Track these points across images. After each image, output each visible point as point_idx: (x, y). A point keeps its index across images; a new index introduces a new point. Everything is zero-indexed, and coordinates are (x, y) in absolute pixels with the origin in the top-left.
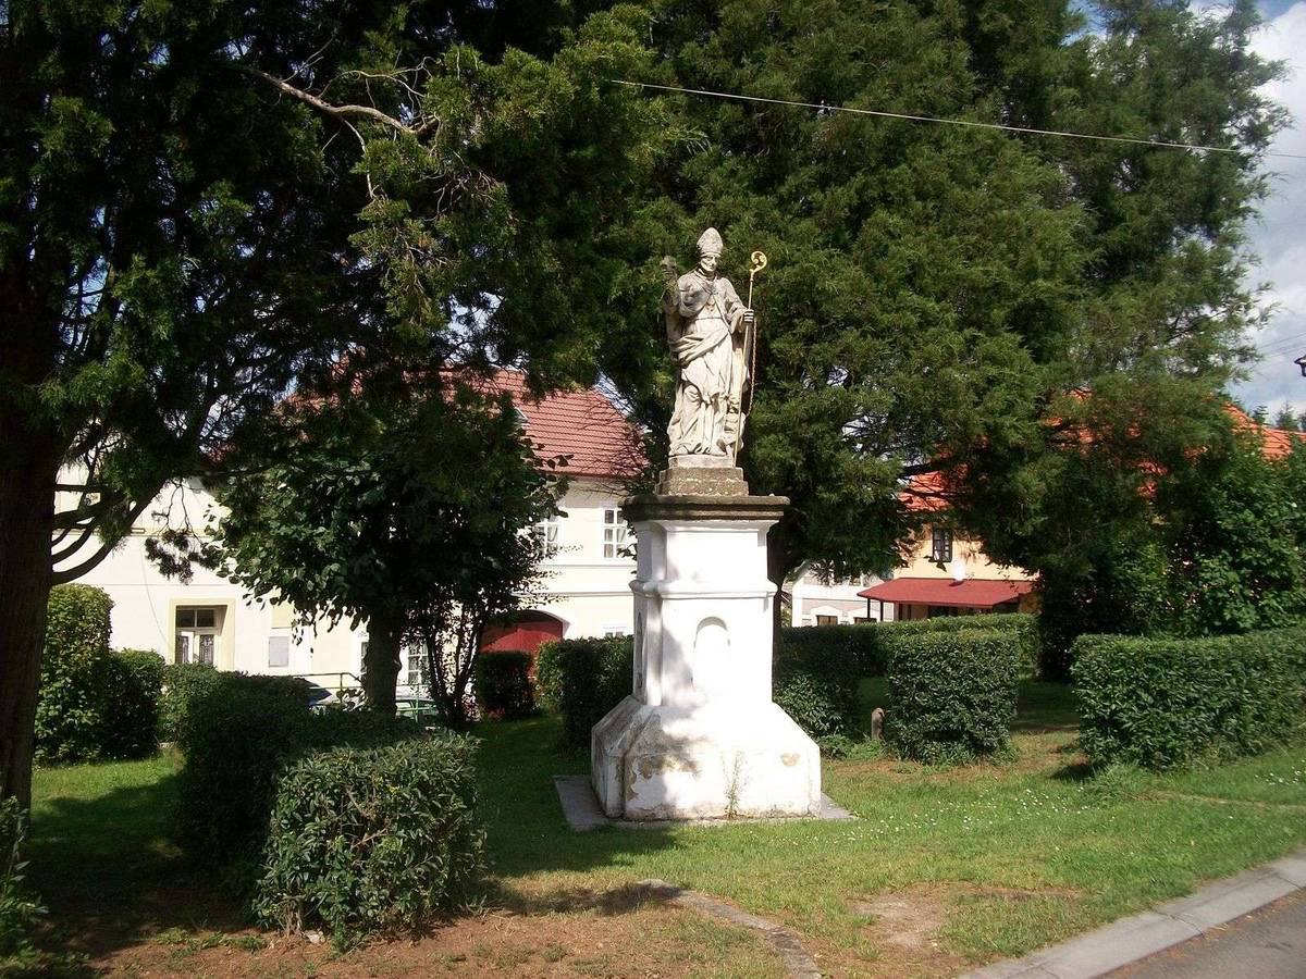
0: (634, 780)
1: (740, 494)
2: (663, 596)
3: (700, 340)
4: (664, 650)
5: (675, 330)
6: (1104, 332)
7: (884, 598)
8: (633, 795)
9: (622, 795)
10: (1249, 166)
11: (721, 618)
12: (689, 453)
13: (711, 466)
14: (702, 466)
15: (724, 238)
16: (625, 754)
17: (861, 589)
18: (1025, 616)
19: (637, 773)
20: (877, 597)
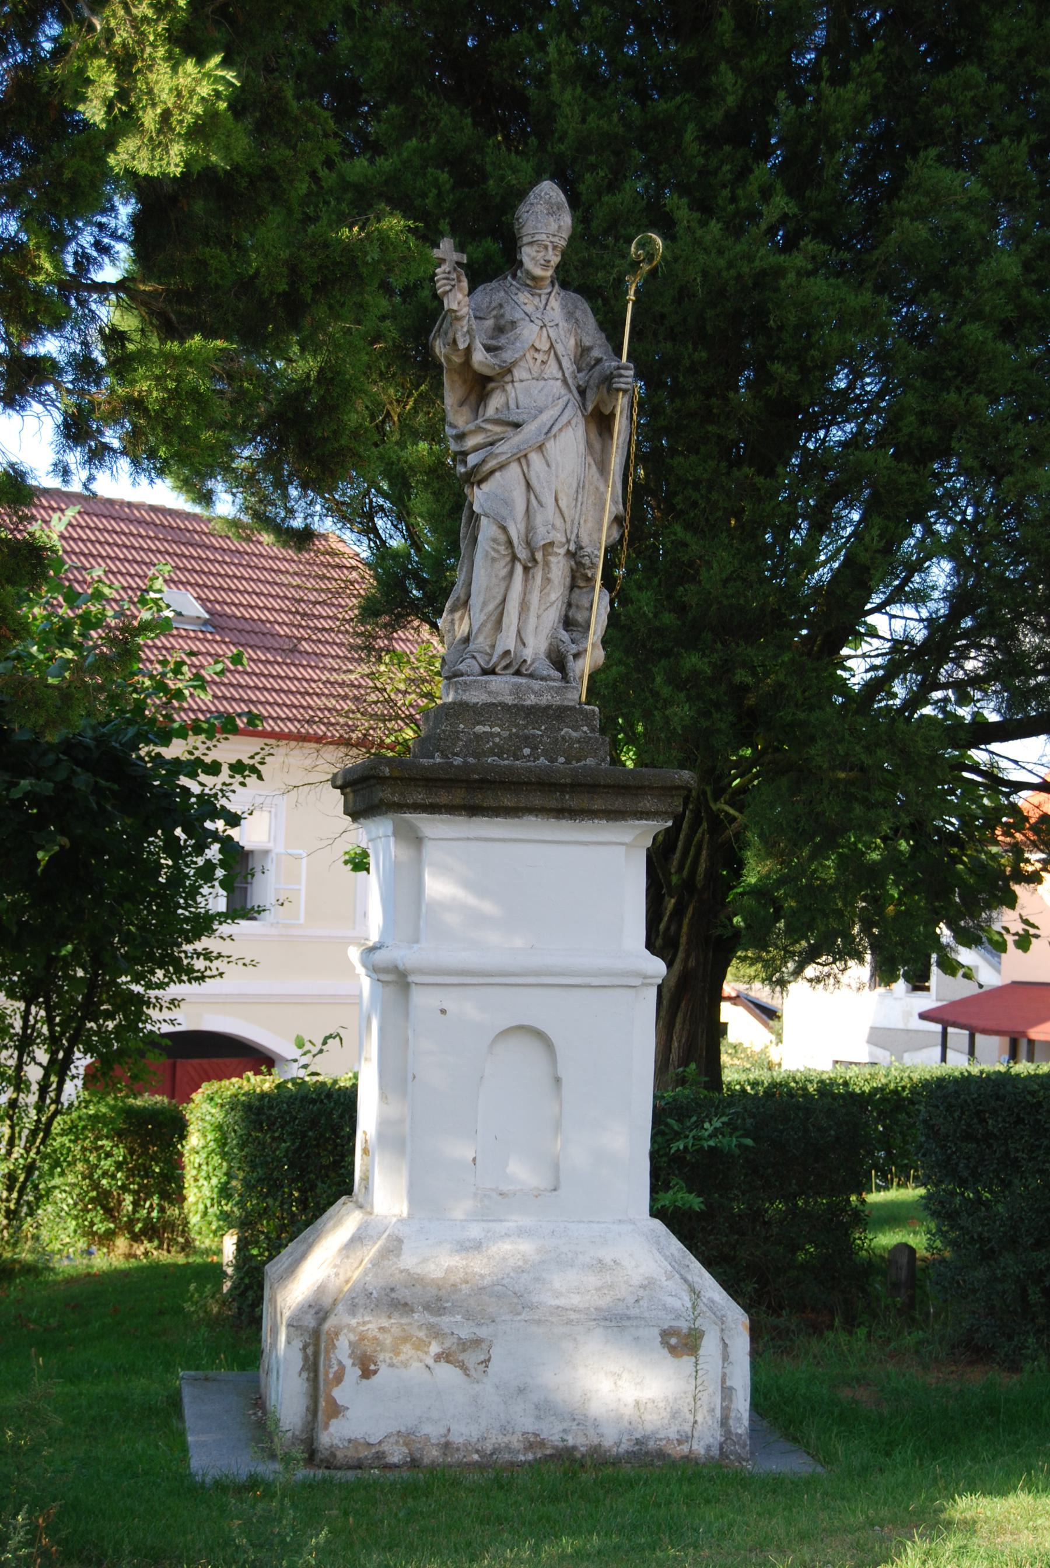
0: (339, 1378)
1: (590, 761)
2: (411, 979)
3: (517, 425)
4: (497, 474)
5: (462, 404)
6: (839, 245)
7: (975, 1023)
8: (336, 1410)
9: (313, 1410)
10: (130, 377)
11: (555, 1039)
12: (485, 672)
13: (531, 700)
14: (509, 700)
15: (574, 201)
16: (320, 1324)
17: (926, 1001)
18: (526, 240)
19: (348, 1362)
20: (963, 1020)
